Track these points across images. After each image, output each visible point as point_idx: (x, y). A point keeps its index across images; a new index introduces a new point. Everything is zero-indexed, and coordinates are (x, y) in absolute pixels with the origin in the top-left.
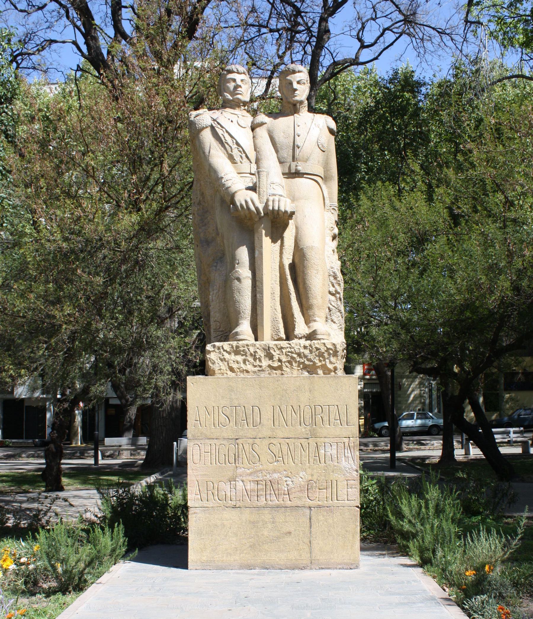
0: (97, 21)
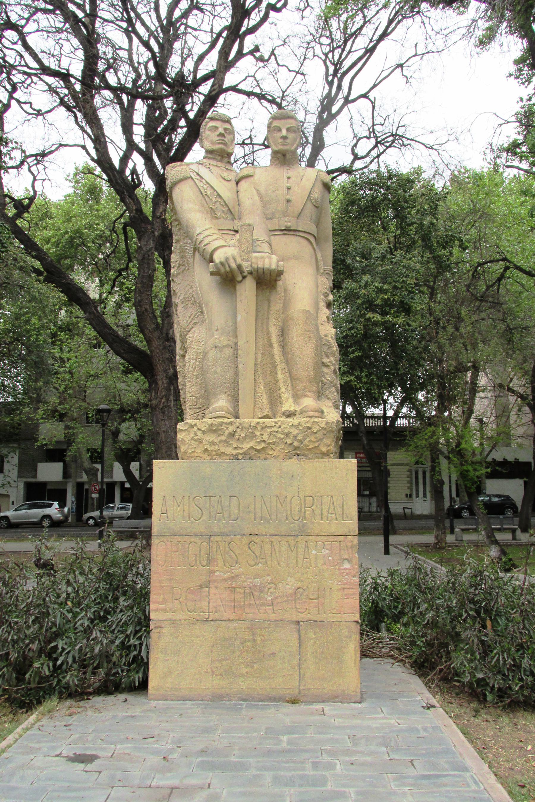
0: (108, 131)
